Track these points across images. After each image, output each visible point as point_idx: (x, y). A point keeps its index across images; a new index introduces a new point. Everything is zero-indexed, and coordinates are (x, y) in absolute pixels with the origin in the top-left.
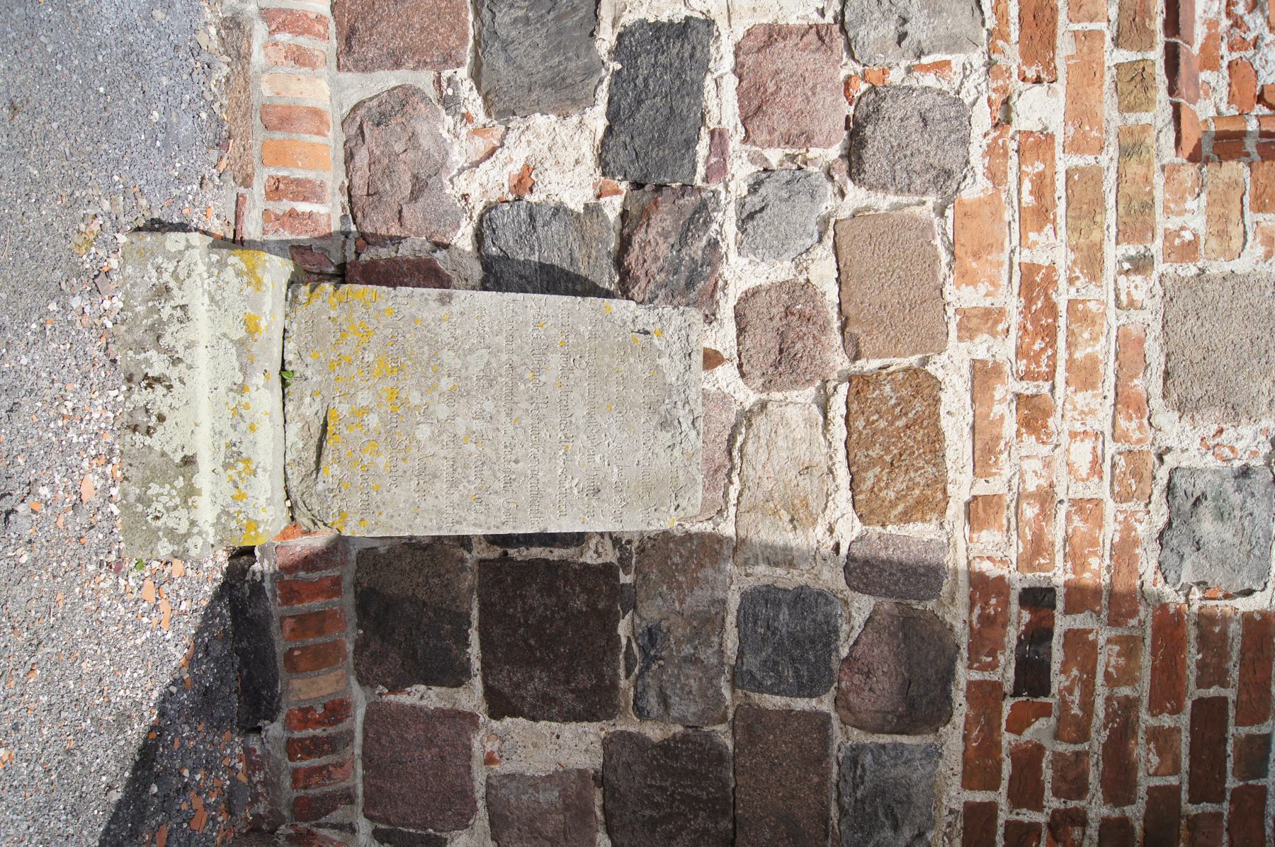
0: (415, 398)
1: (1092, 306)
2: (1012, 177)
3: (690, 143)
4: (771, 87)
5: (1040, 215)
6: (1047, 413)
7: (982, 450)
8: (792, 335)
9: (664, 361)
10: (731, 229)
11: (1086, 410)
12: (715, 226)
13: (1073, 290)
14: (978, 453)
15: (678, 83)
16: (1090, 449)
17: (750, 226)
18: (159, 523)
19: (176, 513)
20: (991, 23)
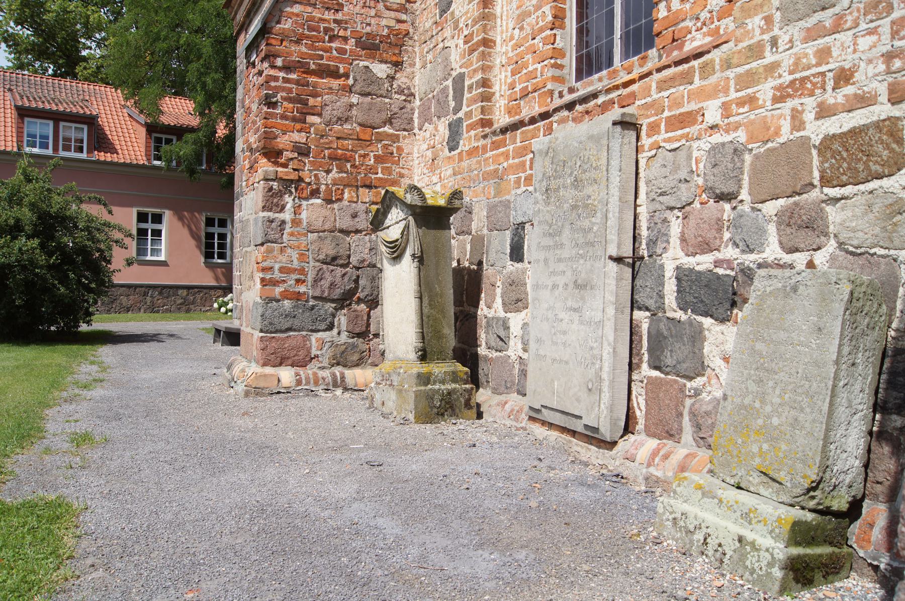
0: (760, 422)
1: (791, 62)
2: (737, 118)
3: (718, 277)
4: (700, 239)
5: (751, 101)
6: (842, 69)
7: (861, 103)
8: (799, 222)
9: (768, 289)
10: (752, 257)
11: (841, 48)
12: (751, 265)
13: (784, 74)
14: (863, 105)
15: (696, 283)
16: (863, 38)
17: (752, 247)
18: (764, 569)
19: (761, 557)
20: (683, 141)
